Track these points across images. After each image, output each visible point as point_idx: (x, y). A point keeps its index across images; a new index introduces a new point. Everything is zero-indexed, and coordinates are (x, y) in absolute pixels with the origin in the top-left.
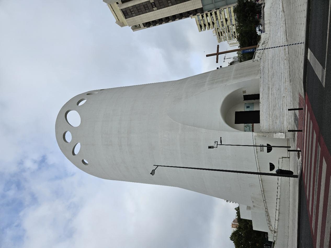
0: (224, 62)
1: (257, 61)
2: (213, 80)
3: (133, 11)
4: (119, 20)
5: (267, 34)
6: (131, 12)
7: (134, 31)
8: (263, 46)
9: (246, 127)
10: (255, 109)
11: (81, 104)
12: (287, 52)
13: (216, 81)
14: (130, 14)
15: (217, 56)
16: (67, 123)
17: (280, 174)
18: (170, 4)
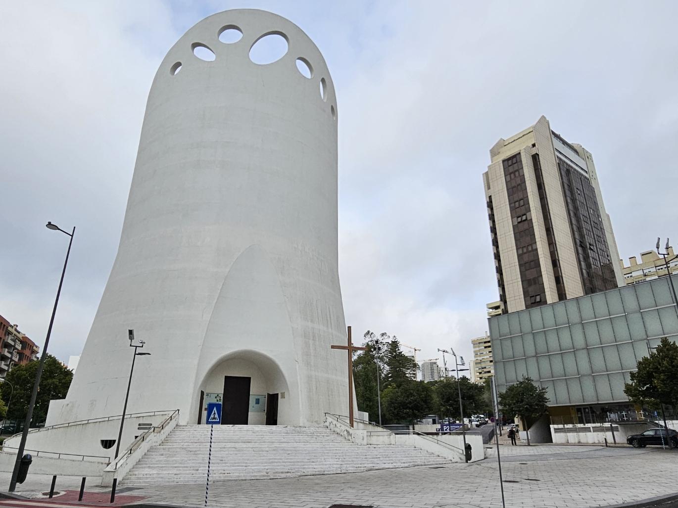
0: (439, 350)
1: (325, 421)
2: (314, 336)
3: (515, 175)
4: (505, 146)
5: (363, 439)
6: (514, 172)
7: (483, 174)
8: (345, 431)
9: (216, 397)
10: (251, 415)
11: (302, 66)
12: (279, 476)
13: (311, 342)
14: (511, 169)
15: (346, 347)
16: (260, 35)
17: (20, 461)
18: (520, 252)
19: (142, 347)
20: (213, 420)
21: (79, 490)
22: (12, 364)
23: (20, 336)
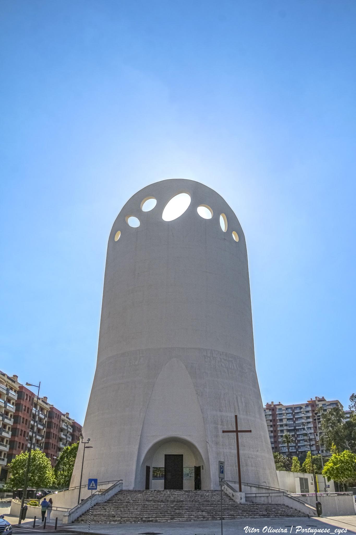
2: (222, 422)
19: (88, 443)
20: (92, 488)
21: (55, 525)
22: (68, 443)
23: (71, 422)
